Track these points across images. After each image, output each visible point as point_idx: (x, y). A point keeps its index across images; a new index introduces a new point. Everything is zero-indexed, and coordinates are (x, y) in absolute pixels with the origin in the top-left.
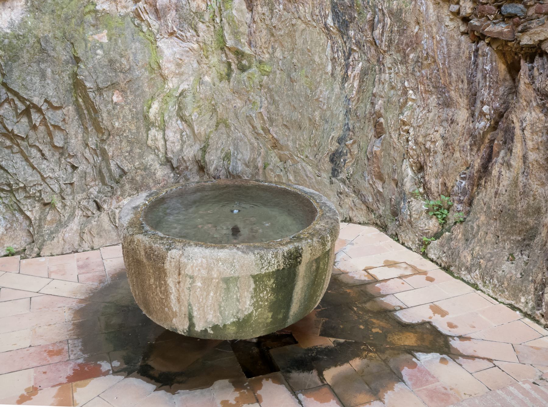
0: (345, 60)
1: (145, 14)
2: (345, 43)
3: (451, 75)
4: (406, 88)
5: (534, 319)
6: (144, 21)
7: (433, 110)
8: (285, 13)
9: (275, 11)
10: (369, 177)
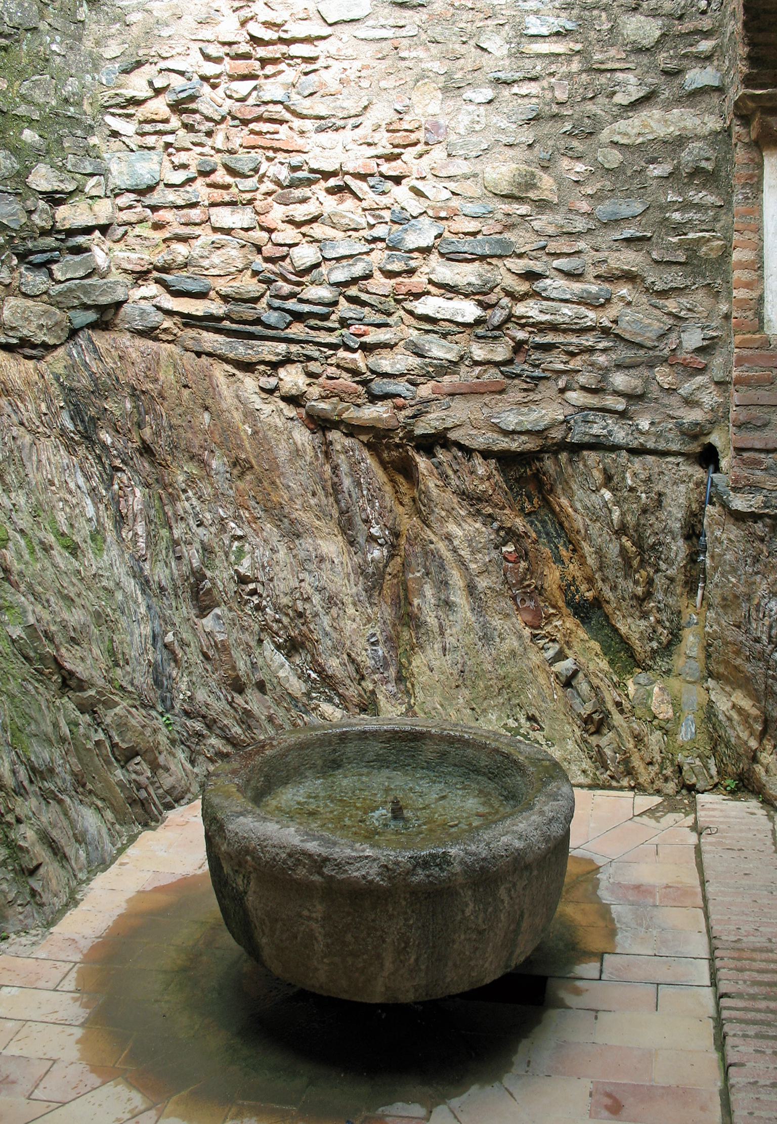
4: (222, 519)
5: (603, 788)
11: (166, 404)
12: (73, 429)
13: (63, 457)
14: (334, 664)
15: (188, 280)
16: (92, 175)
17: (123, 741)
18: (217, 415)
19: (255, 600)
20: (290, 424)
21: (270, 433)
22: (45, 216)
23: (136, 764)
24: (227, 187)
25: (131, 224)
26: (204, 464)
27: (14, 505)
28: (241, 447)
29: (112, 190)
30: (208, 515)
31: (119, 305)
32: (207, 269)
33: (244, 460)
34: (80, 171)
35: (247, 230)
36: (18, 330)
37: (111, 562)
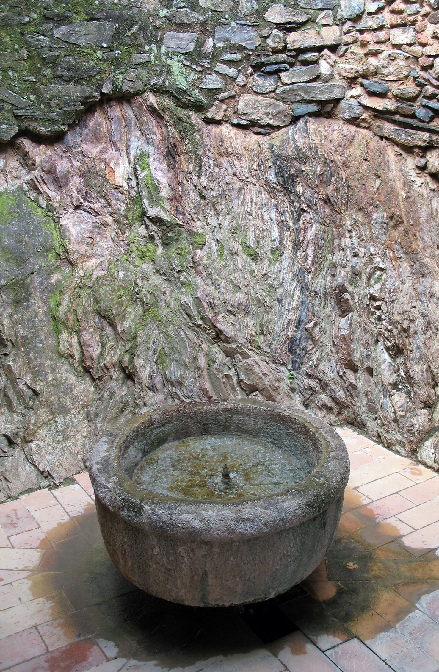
0: (294, 223)
1: (43, 185)
2: (293, 202)
3: (424, 239)
6: (42, 193)
7: (407, 281)
8: (217, 170)
9: (203, 168)
10: (338, 367)
11: (348, 171)
12: (275, 181)
13: (264, 197)
14: (417, 370)
15: (375, 84)
16: (322, 9)
17: (248, 379)
18: (385, 183)
19: (378, 313)
20: (432, 194)
21: (418, 199)
22: (277, 40)
23: (254, 395)
24: (401, 12)
25: (350, 44)
26: (368, 215)
27: (220, 225)
28: (397, 206)
29: (340, 20)
30: (363, 250)
31: (337, 101)
32: (387, 76)
33: (398, 216)
34: (312, 7)
35: (410, 45)
36: (248, 115)
37: (283, 270)
